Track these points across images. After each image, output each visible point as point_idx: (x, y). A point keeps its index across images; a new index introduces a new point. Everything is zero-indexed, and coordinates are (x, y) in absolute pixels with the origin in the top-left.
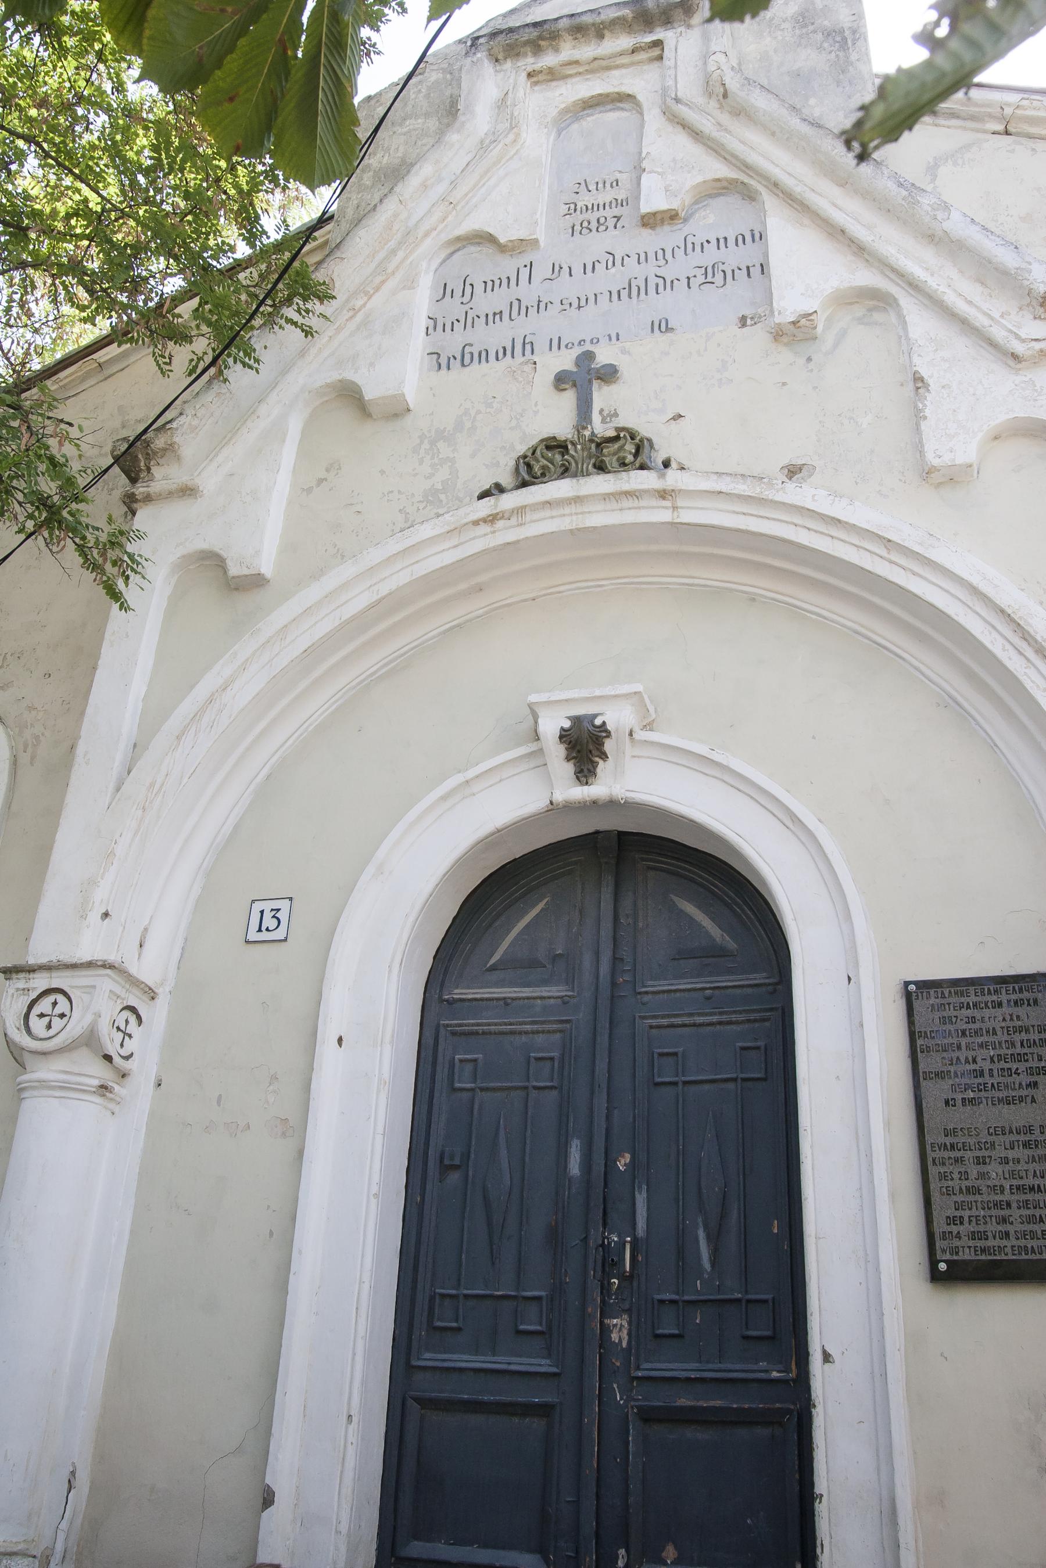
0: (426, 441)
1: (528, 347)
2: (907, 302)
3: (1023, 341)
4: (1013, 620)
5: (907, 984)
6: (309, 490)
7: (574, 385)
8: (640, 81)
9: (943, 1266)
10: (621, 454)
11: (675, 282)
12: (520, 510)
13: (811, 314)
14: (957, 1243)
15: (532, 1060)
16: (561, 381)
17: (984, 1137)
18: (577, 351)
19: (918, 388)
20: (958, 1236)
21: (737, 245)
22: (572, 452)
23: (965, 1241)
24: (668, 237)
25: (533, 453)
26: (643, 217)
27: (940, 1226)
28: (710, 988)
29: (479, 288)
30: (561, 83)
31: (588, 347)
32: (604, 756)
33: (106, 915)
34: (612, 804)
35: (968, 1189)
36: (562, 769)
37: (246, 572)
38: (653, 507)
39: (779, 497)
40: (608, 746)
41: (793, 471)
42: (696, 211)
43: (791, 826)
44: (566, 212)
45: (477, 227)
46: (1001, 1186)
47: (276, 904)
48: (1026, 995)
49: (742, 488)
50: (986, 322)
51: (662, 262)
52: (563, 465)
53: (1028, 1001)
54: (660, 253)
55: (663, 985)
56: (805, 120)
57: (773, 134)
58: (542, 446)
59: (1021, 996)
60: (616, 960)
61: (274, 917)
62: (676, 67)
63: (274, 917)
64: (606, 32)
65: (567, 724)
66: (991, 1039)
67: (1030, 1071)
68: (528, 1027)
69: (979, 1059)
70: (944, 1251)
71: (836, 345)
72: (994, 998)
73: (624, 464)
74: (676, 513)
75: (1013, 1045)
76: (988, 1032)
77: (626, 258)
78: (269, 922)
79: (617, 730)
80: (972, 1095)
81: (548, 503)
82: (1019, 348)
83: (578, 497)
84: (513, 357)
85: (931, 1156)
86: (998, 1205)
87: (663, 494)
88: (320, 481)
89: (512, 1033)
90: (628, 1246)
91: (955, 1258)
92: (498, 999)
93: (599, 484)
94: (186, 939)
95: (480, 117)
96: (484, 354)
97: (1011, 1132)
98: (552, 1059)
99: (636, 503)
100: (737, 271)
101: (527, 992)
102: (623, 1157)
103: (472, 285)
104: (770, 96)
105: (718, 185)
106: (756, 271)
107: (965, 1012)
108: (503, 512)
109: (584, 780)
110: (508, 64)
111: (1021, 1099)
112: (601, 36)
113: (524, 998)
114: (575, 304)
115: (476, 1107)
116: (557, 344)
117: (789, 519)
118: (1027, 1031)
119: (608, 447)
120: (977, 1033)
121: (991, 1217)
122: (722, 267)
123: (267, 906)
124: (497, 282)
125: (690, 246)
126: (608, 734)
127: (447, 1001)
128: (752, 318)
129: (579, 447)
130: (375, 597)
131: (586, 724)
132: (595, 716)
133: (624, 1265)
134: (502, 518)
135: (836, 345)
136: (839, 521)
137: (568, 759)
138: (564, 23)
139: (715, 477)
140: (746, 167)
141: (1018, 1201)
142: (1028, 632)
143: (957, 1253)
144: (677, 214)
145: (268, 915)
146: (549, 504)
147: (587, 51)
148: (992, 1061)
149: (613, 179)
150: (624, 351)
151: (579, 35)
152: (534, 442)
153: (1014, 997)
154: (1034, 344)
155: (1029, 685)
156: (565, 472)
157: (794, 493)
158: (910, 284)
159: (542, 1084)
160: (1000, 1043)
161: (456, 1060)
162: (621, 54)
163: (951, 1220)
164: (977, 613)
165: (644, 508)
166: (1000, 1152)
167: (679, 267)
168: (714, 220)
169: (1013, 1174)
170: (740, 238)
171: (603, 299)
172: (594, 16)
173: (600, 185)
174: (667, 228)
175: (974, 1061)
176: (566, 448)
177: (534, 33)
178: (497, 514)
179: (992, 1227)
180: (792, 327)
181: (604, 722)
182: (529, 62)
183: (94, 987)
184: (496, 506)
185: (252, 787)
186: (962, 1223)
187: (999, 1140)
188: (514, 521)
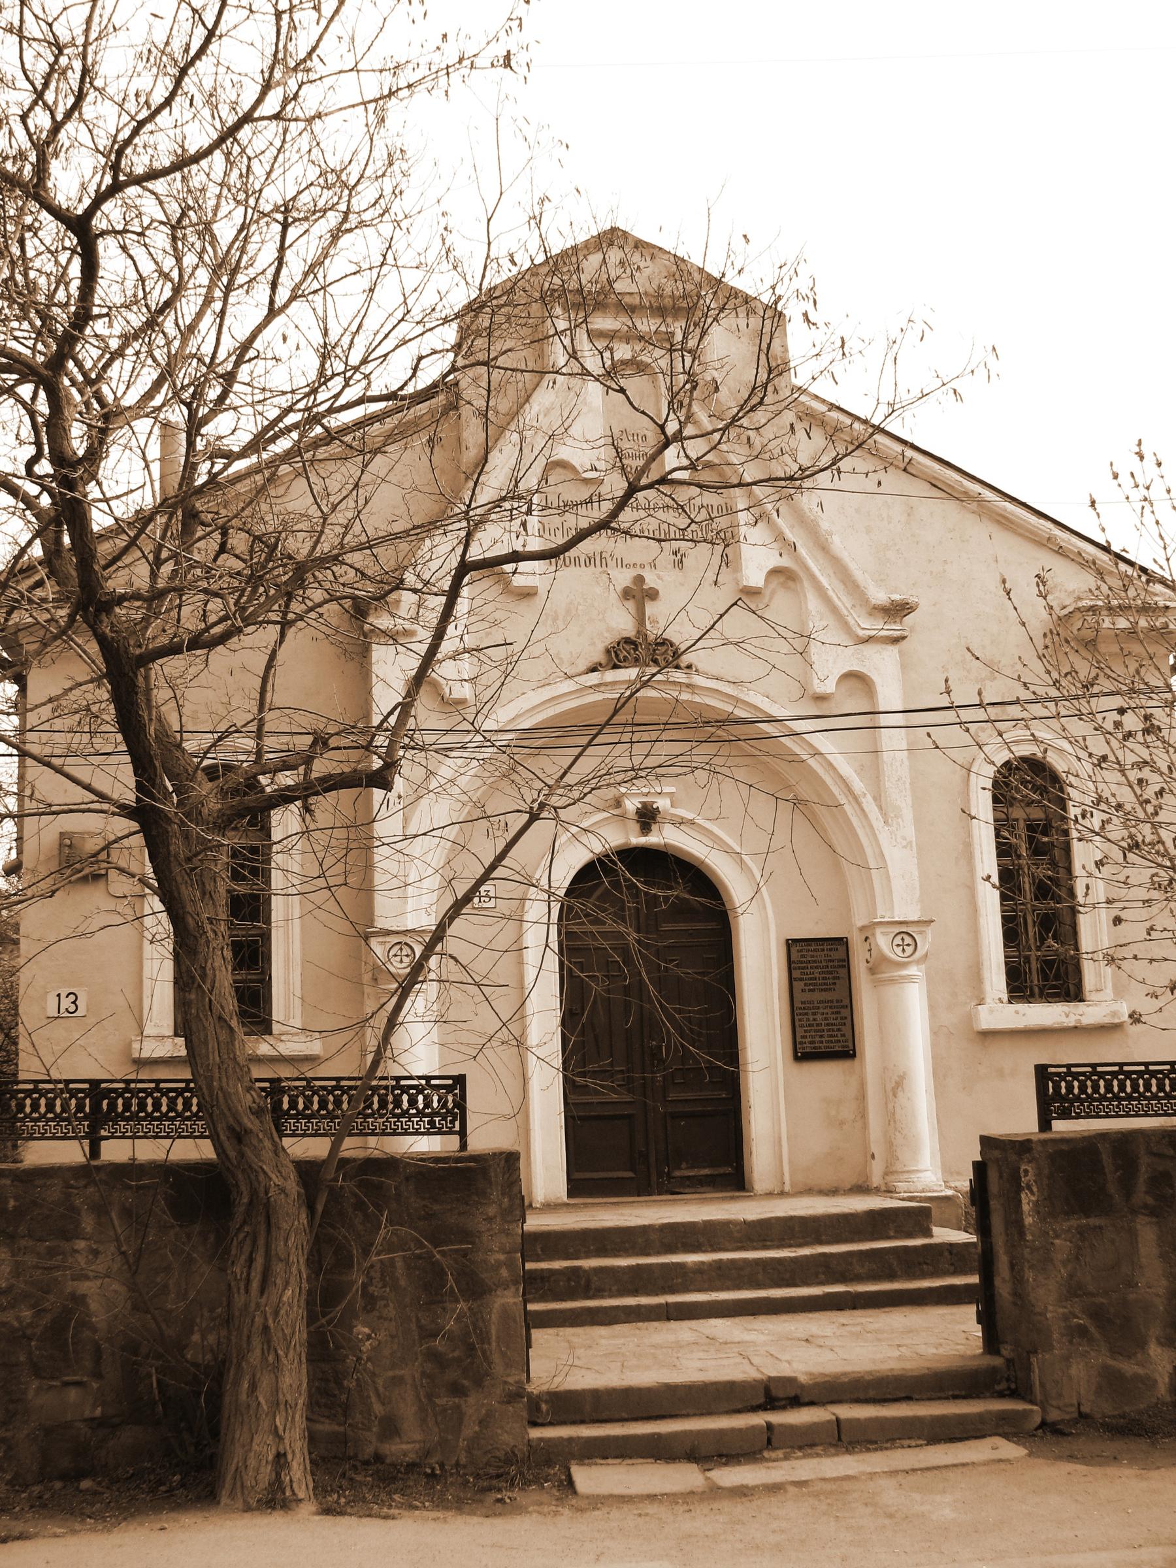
2: (806, 584)
16: (627, 594)
18: (632, 573)
27: (799, 1039)
36: (635, 827)
65: (640, 806)
67: (834, 978)
86: (819, 1031)
116: (621, 563)
120: (815, 962)
163: (803, 1037)
166: (821, 1010)
169: (826, 1019)
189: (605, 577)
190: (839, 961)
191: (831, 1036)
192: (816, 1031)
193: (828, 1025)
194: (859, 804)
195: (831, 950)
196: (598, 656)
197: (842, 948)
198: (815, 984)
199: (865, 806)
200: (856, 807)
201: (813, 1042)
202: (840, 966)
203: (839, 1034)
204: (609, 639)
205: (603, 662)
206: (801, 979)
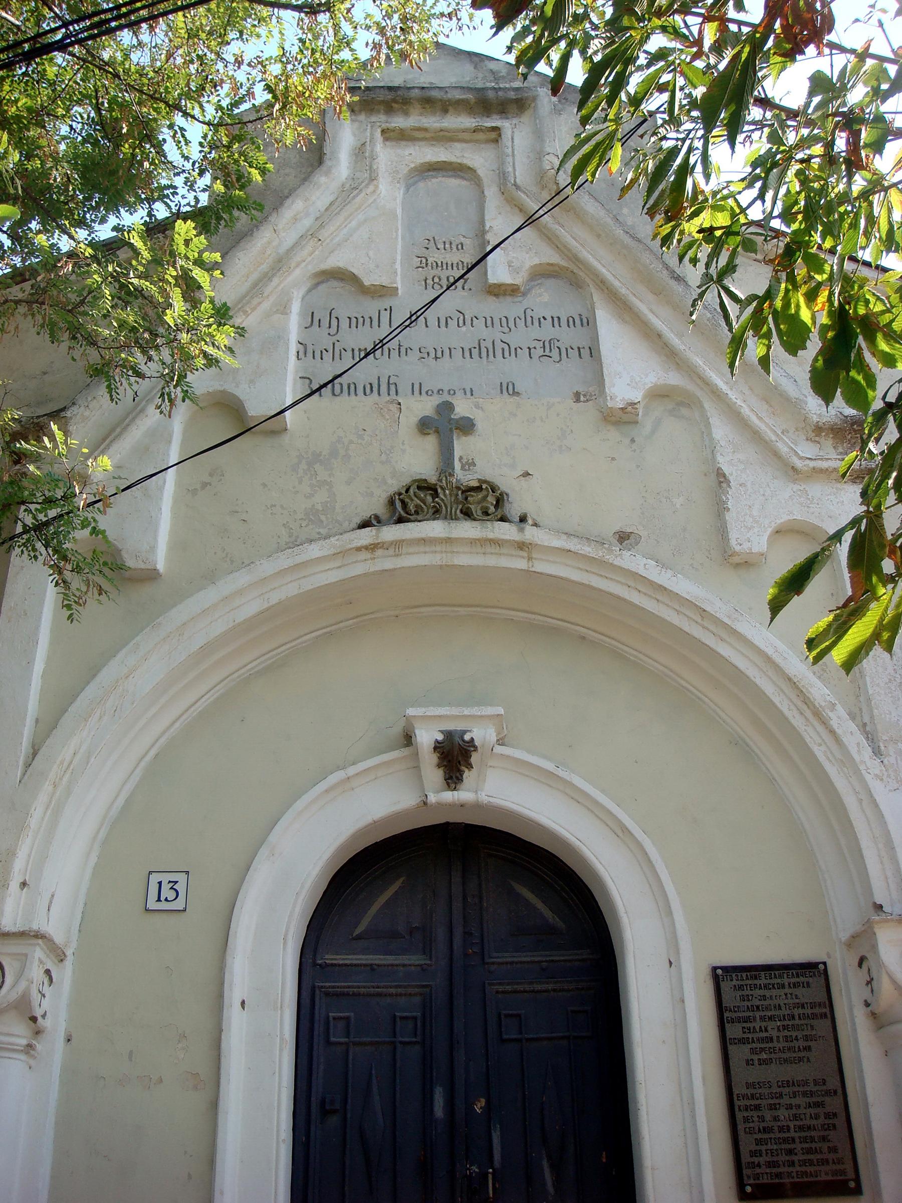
0: (304, 461)
1: (393, 387)
3: (801, 458)
4: (798, 688)
5: (715, 969)
6: (194, 492)
7: (437, 431)
8: (478, 158)
9: (749, 1189)
10: (484, 504)
11: (519, 350)
12: (398, 544)
13: (635, 404)
14: (758, 1170)
15: (398, 1019)
16: (424, 426)
17: (775, 1090)
18: (436, 400)
19: (721, 482)
20: (759, 1165)
21: (569, 326)
22: (442, 496)
23: (763, 1169)
24: (510, 308)
25: (407, 491)
26: (490, 286)
27: (746, 1158)
28: (546, 961)
29: (344, 324)
30: (410, 143)
31: (446, 397)
32: (470, 766)
33: (24, 884)
34: (478, 806)
35: (764, 1128)
36: (433, 774)
37: (143, 566)
38: (512, 555)
39: (618, 562)
40: (474, 758)
41: (623, 537)
42: (532, 288)
43: (621, 835)
44: (419, 265)
45: (341, 265)
46: (788, 1126)
47: (173, 877)
48: (801, 979)
49: (587, 550)
50: (774, 438)
51: (506, 330)
52: (434, 507)
53: (803, 983)
54: (504, 320)
55: (507, 957)
56: (627, 233)
57: (599, 236)
58: (415, 486)
59: (798, 980)
60: (467, 934)
61: (172, 888)
62: (513, 155)
63: (172, 888)
64: (450, 108)
65: (440, 737)
66: (777, 1013)
67: (806, 1038)
68: (393, 991)
69: (769, 1029)
70: (749, 1177)
71: (653, 432)
72: (779, 981)
73: (486, 513)
74: (531, 564)
75: (793, 1018)
76: (775, 1007)
77: (474, 319)
78: (166, 893)
79: (483, 746)
80: (765, 1056)
81: (424, 540)
82: (799, 464)
83: (450, 538)
84: (379, 394)
85: (737, 1103)
86: (785, 1141)
87: (522, 546)
88: (205, 485)
89: (380, 995)
90: (490, 1176)
91: (757, 1182)
92: (365, 965)
93: (467, 529)
94: (85, 904)
95: (342, 164)
96: (352, 386)
97: (793, 1084)
98: (415, 1018)
99: (497, 550)
100: (570, 350)
101: (390, 959)
102: (479, 1101)
103: (337, 318)
104: (597, 204)
105: (551, 268)
106: (585, 353)
107: (758, 992)
108: (384, 543)
109: (453, 786)
110: (362, 117)
111: (801, 1059)
112: (445, 111)
113: (388, 966)
114: (432, 355)
115: (351, 1057)
116: (418, 389)
117: (624, 581)
118: (803, 1007)
119: (473, 496)
120: (768, 1008)
121: (781, 1149)
122: (557, 344)
123: (165, 878)
124: (361, 320)
125: (529, 320)
126: (476, 748)
127: (320, 965)
128: (585, 396)
129: (447, 492)
130: (266, 606)
131: (457, 739)
132: (465, 732)
133: (488, 1193)
134: (382, 547)
135: (653, 432)
136: (665, 589)
137: (439, 766)
138: (416, 93)
139: (565, 537)
140: (575, 258)
141: (800, 1137)
142: (808, 698)
143: (758, 1179)
144: (519, 289)
145: (165, 887)
146: (424, 541)
147: (433, 122)
148: (779, 1030)
149: (458, 242)
150: (477, 406)
151: (427, 106)
152: (406, 481)
153: (793, 980)
154: (808, 462)
155: (808, 740)
156: (436, 513)
157: (629, 560)
158: (713, 392)
159: (407, 1039)
160: (784, 1016)
161: (331, 1019)
162: (464, 131)
163: (753, 1154)
164: (770, 678)
165: (504, 554)
166: (786, 1100)
167: (520, 337)
168: (544, 300)
169: (795, 1117)
170: (571, 320)
171: (457, 354)
172: (442, 93)
173: (447, 246)
174: (509, 299)
175: (766, 1030)
176: (436, 491)
177: (390, 96)
178: (378, 544)
179: (783, 1158)
180: (621, 412)
181: (472, 739)
182: (380, 119)
183: (26, 955)
184: (377, 536)
185: (143, 764)
186: (761, 1156)
187: (786, 1090)
188: (391, 551)
189: (394, 407)
190: (813, 1005)
191: (809, 1151)
192: (779, 1141)
193: (801, 1128)
194: (824, 722)
195: (795, 985)
196: (377, 505)
197: (816, 982)
198: (772, 1050)
199: (834, 723)
200: (820, 728)
201: (774, 1164)
202: (814, 1016)
203: (825, 1146)
204: (395, 485)
205: (384, 516)
206: (743, 1041)
